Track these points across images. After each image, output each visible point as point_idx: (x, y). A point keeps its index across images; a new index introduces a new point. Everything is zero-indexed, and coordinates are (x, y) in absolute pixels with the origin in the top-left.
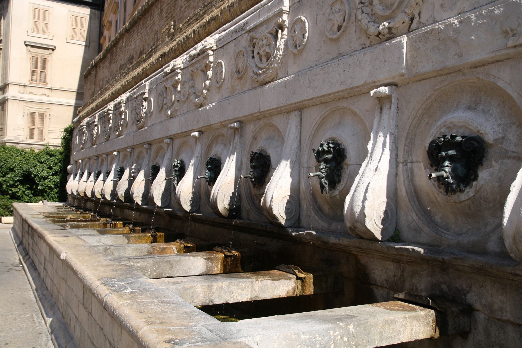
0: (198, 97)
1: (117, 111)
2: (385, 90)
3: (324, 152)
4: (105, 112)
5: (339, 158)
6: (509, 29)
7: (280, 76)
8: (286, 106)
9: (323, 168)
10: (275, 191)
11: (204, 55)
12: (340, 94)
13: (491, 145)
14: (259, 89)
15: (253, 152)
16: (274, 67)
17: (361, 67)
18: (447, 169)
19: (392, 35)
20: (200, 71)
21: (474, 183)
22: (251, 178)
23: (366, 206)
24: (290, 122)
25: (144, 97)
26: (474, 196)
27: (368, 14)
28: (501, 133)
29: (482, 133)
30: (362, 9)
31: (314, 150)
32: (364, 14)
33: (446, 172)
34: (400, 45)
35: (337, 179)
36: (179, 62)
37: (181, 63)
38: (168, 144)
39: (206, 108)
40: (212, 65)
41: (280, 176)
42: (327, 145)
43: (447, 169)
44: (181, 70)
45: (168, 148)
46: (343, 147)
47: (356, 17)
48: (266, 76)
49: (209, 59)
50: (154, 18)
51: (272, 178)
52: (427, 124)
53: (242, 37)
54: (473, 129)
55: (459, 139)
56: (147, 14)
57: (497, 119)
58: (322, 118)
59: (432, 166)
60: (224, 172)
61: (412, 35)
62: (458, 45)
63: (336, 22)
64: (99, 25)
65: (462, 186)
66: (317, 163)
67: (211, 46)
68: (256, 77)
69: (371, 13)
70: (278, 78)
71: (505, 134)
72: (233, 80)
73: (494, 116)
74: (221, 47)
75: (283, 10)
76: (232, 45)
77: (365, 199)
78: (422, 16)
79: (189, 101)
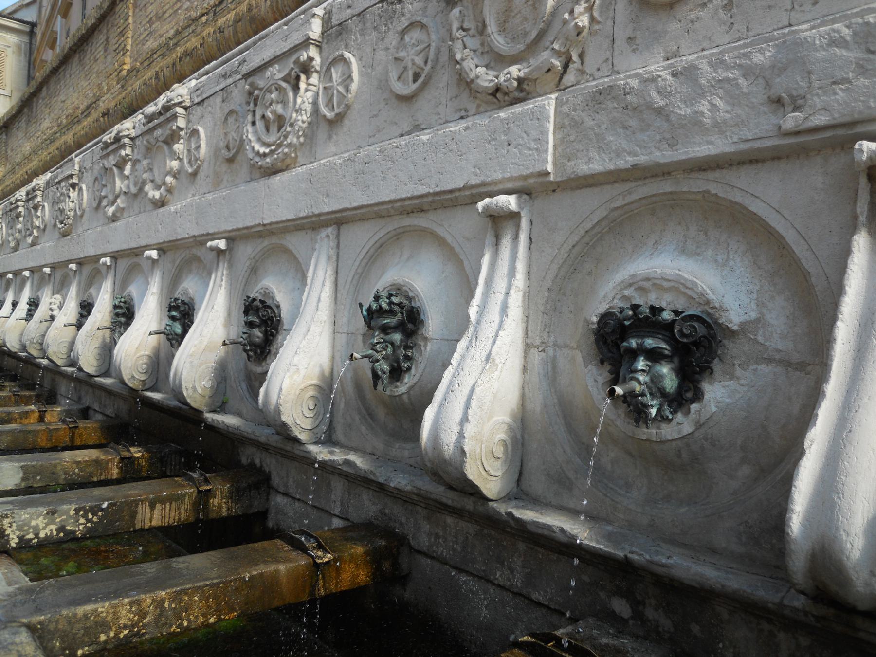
0: (158, 188)
1: (31, 202)
2: (510, 202)
3: (380, 311)
4: (11, 204)
5: (410, 326)
6: (783, 95)
7: (683, 51)
8: (311, 217)
9: (378, 343)
10: (286, 376)
11: (168, 115)
12: (416, 201)
13: (733, 334)
14: (262, 182)
15: (248, 297)
16: (290, 143)
17: (459, 153)
18: (642, 378)
19: (522, 95)
20: (161, 144)
21: (694, 407)
22: (245, 345)
23: (466, 435)
24: (317, 246)
25: (71, 181)
26: (692, 433)
27: (475, 51)
28: (753, 311)
29: (716, 308)
30: (462, 40)
31: (361, 305)
32: (467, 50)
33: (639, 382)
34: (539, 117)
35: (405, 365)
36: (128, 126)
37: (132, 127)
38: (108, 266)
39: (170, 209)
40: (182, 133)
41: (295, 348)
42: (387, 298)
43: (642, 378)
44: (132, 139)
45: (108, 272)
46: (418, 304)
47: (452, 56)
48: (275, 159)
49: (176, 122)
50: (96, 50)
51: (281, 350)
52: (590, 274)
53: (236, 86)
54: (695, 296)
55: (667, 316)
56: (85, 44)
57: (746, 280)
58: (378, 245)
59: (602, 362)
60: (197, 327)
61: (566, 96)
62: (668, 120)
63: (410, 65)
64: (27, 64)
65: (667, 412)
66: (367, 328)
67: (182, 100)
68: (257, 159)
69: (480, 51)
70: (298, 165)
71: (761, 313)
72: (218, 163)
73: (738, 272)
74: (198, 104)
75: (309, 38)
76: (218, 99)
77: (465, 419)
78: (587, 59)
79: (143, 194)
